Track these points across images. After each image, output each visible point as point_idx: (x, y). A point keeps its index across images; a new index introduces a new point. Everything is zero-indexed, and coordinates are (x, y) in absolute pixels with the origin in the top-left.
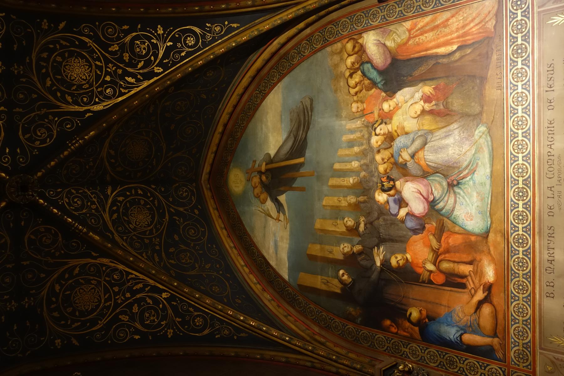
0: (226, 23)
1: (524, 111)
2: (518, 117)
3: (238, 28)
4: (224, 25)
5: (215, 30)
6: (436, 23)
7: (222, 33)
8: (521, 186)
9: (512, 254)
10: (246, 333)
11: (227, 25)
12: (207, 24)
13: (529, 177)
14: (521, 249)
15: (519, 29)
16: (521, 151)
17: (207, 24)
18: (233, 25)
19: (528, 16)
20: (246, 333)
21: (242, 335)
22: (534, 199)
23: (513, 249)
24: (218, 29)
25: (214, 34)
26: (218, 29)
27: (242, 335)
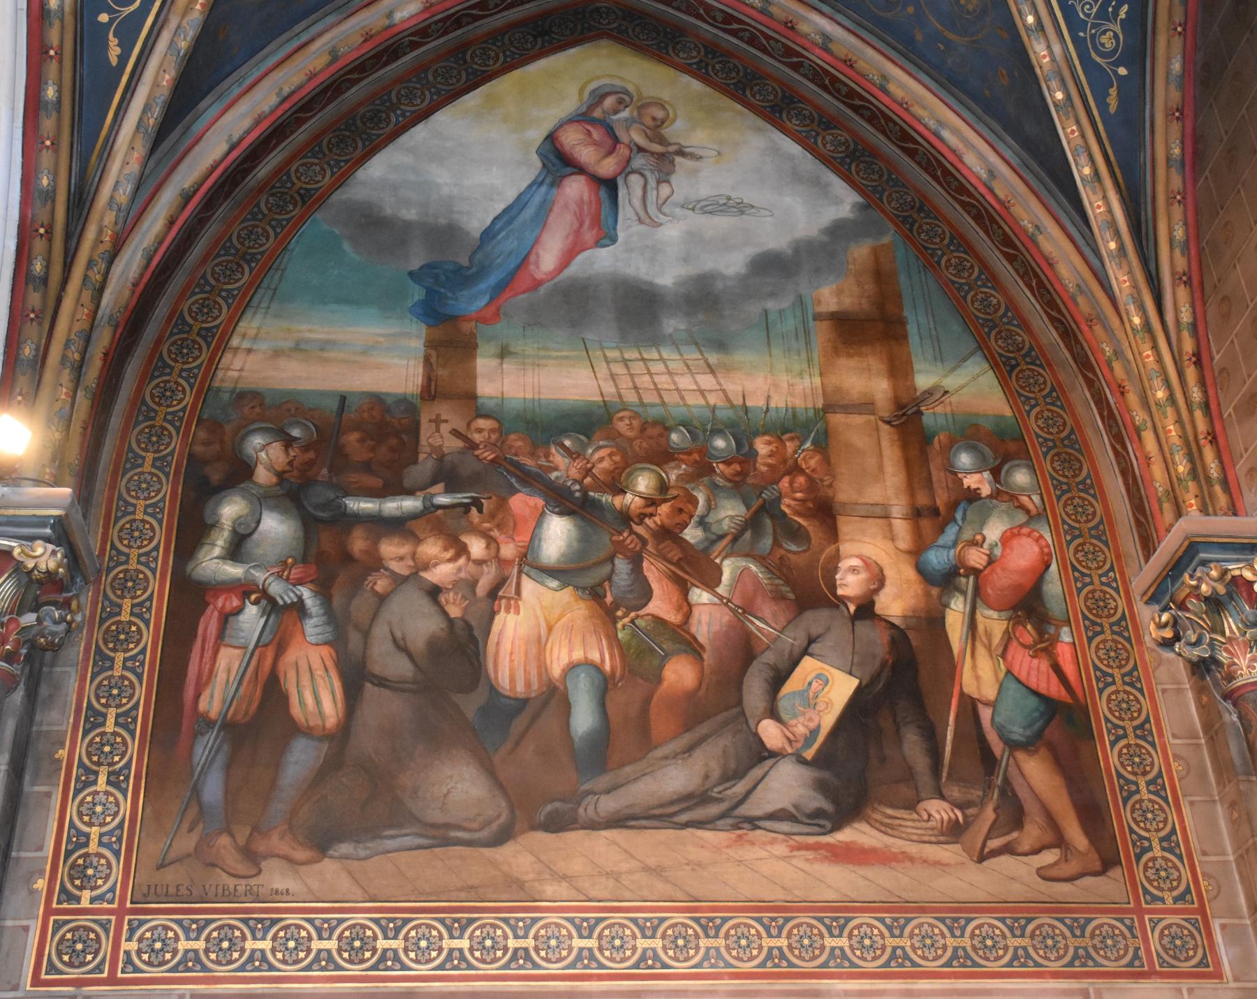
0: (1122, 71)
1: (585, 953)
2: (822, 937)
3: (1103, 106)
4: (1117, 64)
5: (1104, 32)
6: (725, 714)
7: (1093, 55)
8: (180, 947)
9: (252, 923)
10: (123, 59)
11: (1116, 73)
12: (1125, 8)
13: (536, 966)
14: (249, 945)
15: (80, 940)
16: (856, 945)
17: (1125, 8)
18: (1113, 92)
19: (1015, 963)
20: (123, 59)
21: (113, 41)
22: (600, 978)
23: (963, 922)
24: (1107, 41)
25: (1094, 26)
26: (1107, 41)
27: (113, 41)
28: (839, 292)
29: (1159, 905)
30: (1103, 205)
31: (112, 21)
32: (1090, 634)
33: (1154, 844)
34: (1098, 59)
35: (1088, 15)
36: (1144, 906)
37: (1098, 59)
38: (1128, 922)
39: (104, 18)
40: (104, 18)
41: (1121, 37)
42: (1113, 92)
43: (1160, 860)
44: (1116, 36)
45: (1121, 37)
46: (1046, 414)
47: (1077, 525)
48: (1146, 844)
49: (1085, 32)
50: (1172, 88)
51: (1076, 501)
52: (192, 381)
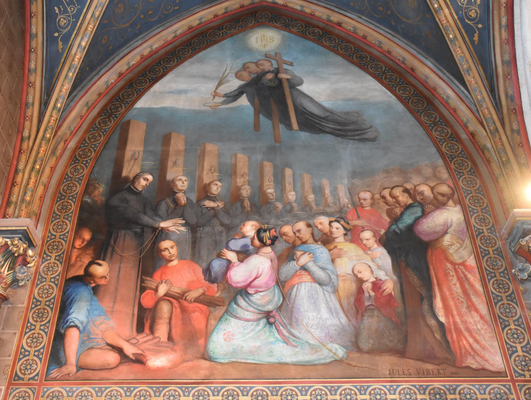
0: (480, 26)
4: (477, 23)
5: (471, 11)
7: (467, 21)
11: (477, 27)
18: (476, 35)
21: (60, 43)
27: (60, 43)
28: (431, 321)
29: (522, 378)
30: (474, 78)
31: (59, 35)
32: (496, 301)
33: (511, 323)
34: (469, 22)
35: (463, 4)
36: (515, 378)
37: (469, 22)
38: (507, 386)
39: (56, 34)
40: (56, 34)
41: (478, 11)
42: (476, 35)
43: (499, 281)
44: (476, 12)
45: (478, 11)
46: (449, 145)
47: (499, 294)
48: (514, 349)
49: (462, 12)
50: (503, 30)
51: (454, 151)
52: (80, 182)
